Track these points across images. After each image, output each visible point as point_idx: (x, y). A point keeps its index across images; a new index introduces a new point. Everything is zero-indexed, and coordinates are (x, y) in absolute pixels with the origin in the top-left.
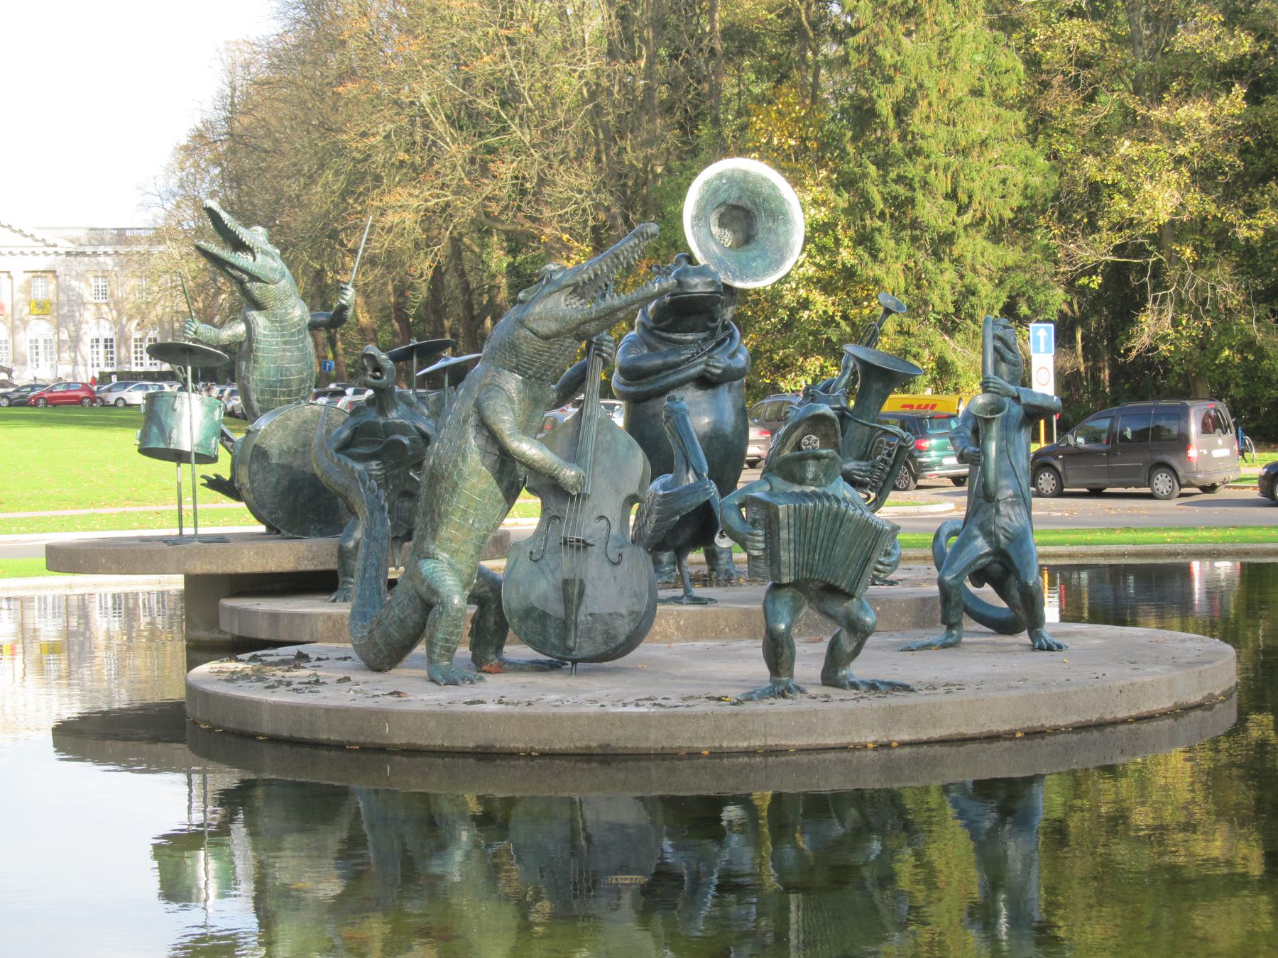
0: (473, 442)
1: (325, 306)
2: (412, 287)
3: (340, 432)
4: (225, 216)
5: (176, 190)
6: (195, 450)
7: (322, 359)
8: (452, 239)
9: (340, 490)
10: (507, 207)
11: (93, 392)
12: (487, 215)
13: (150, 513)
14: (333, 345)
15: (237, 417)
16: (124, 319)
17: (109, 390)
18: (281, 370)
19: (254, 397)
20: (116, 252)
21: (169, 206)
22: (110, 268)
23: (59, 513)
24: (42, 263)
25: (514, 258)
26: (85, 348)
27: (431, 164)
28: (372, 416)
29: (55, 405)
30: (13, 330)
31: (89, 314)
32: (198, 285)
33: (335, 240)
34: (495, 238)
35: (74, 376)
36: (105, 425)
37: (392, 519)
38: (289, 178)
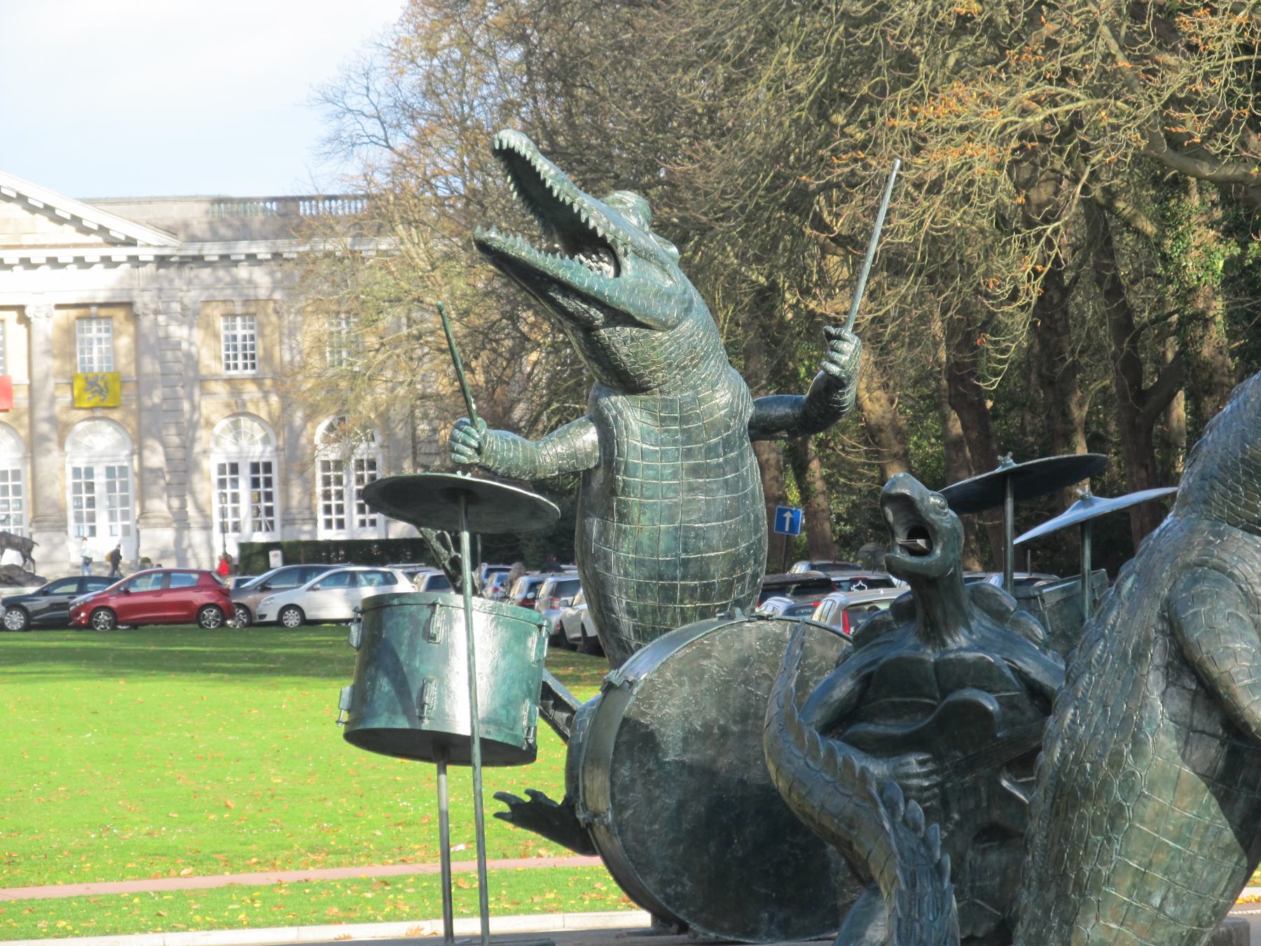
0: (1159, 705)
1: (782, 378)
2: (990, 324)
3: (830, 685)
4: (544, 167)
5: (416, 102)
6: (482, 732)
7: (776, 502)
8: (1088, 203)
9: (831, 825)
10: (1223, 122)
11: (225, 593)
12: (1175, 142)
13: (367, 884)
14: (801, 469)
15: (572, 647)
16: (298, 416)
17: (264, 588)
18: (685, 537)
19: (620, 602)
20: (277, 256)
21: (400, 142)
22: (263, 293)
23: (149, 885)
24: (99, 284)
25: (1244, 246)
26: (207, 488)
27: (1033, 21)
28: (909, 645)
29: (135, 626)
30: (33, 447)
31: (212, 406)
32: (474, 332)
33: (804, 214)
34: (1195, 200)
35: (180, 551)
36: (257, 671)
37: (959, 894)
38: (688, 66)
